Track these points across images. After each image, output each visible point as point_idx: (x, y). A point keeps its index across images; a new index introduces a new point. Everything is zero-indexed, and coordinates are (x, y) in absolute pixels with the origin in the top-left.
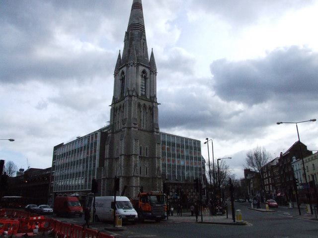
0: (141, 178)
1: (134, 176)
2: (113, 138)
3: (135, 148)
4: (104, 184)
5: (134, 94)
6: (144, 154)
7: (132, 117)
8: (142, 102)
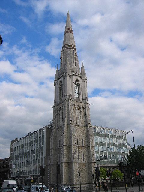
8: (77, 104)
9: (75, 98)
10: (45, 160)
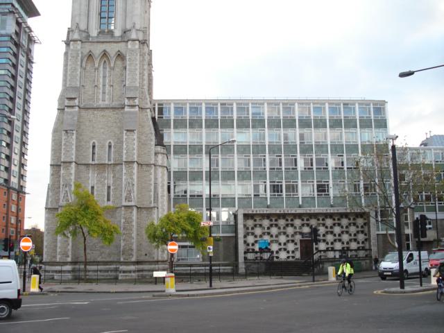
8: (97, 50)
9: (94, 32)
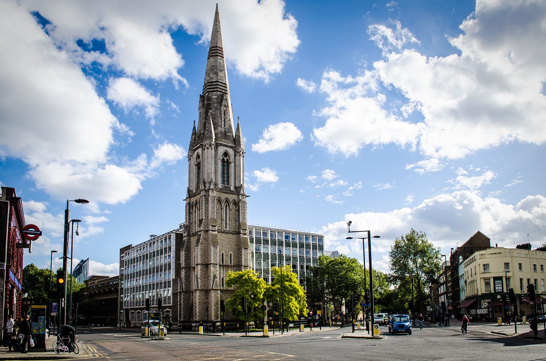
0: (220, 290)
1: (212, 289)
2: (189, 242)
3: (215, 257)
4: (180, 299)
5: (212, 187)
6: (227, 261)
7: (210, 217)
10: (173, 284)
